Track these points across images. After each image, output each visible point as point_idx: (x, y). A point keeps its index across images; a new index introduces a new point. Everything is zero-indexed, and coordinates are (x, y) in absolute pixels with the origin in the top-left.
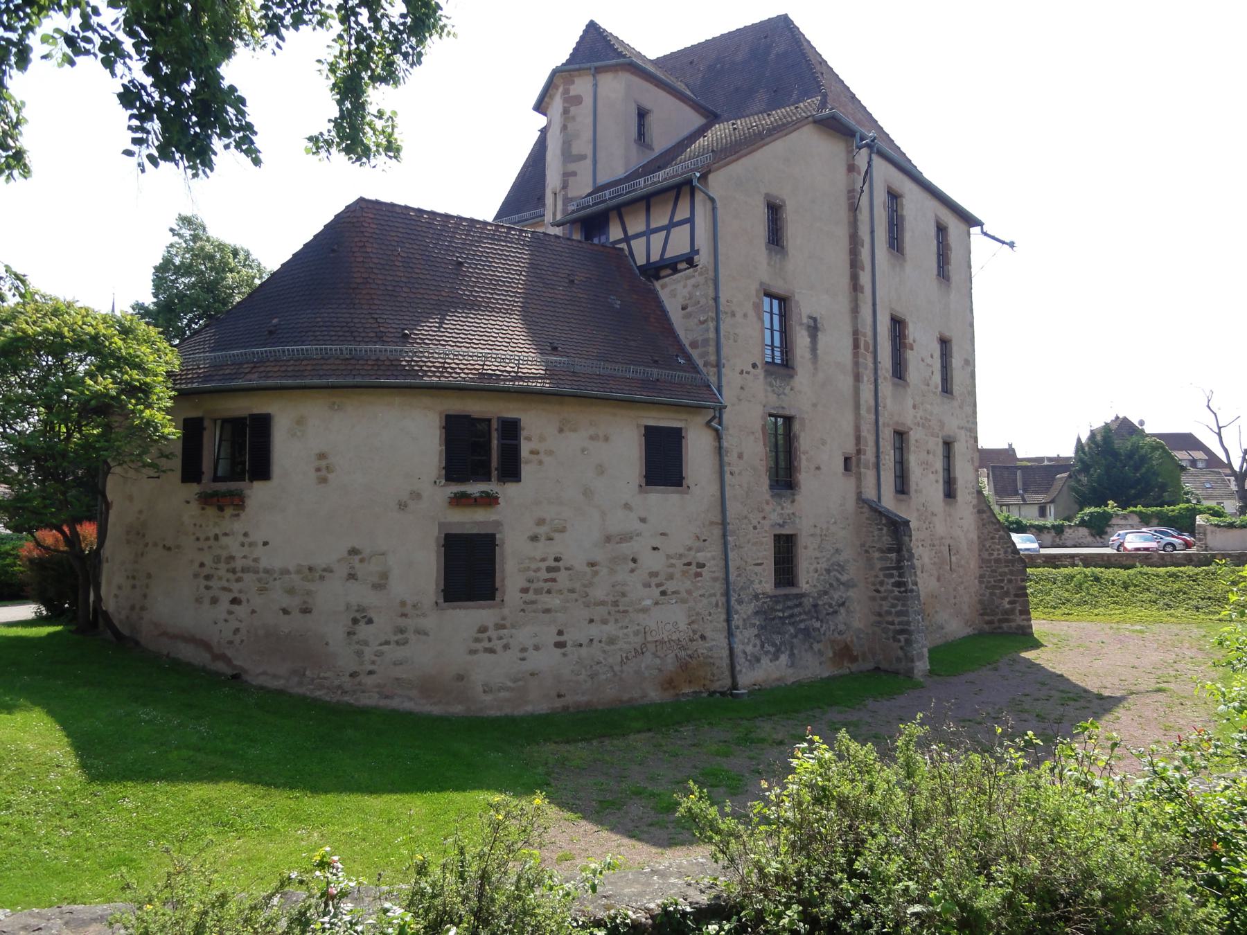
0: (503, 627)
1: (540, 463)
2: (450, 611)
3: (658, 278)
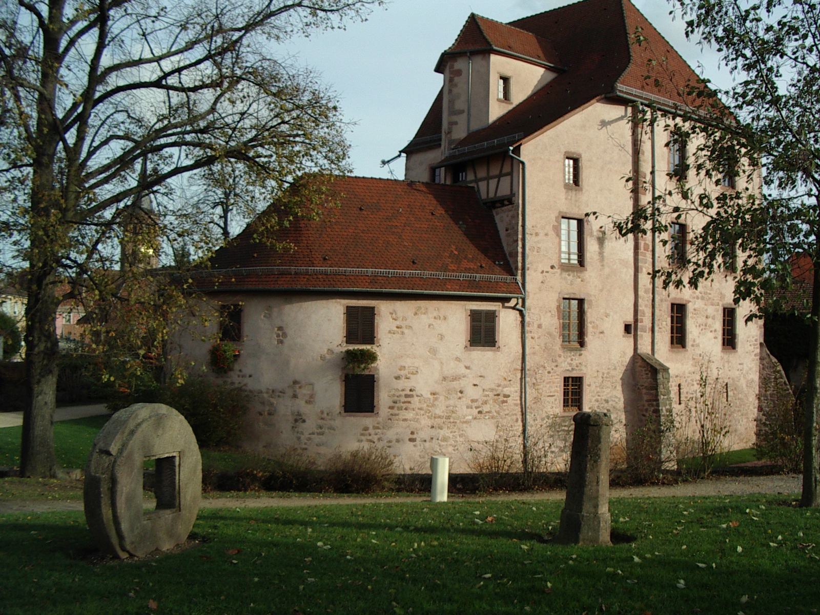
0: (378, 428)
1: (403, 333)
2: (348, 418)
3: (495, 208)
